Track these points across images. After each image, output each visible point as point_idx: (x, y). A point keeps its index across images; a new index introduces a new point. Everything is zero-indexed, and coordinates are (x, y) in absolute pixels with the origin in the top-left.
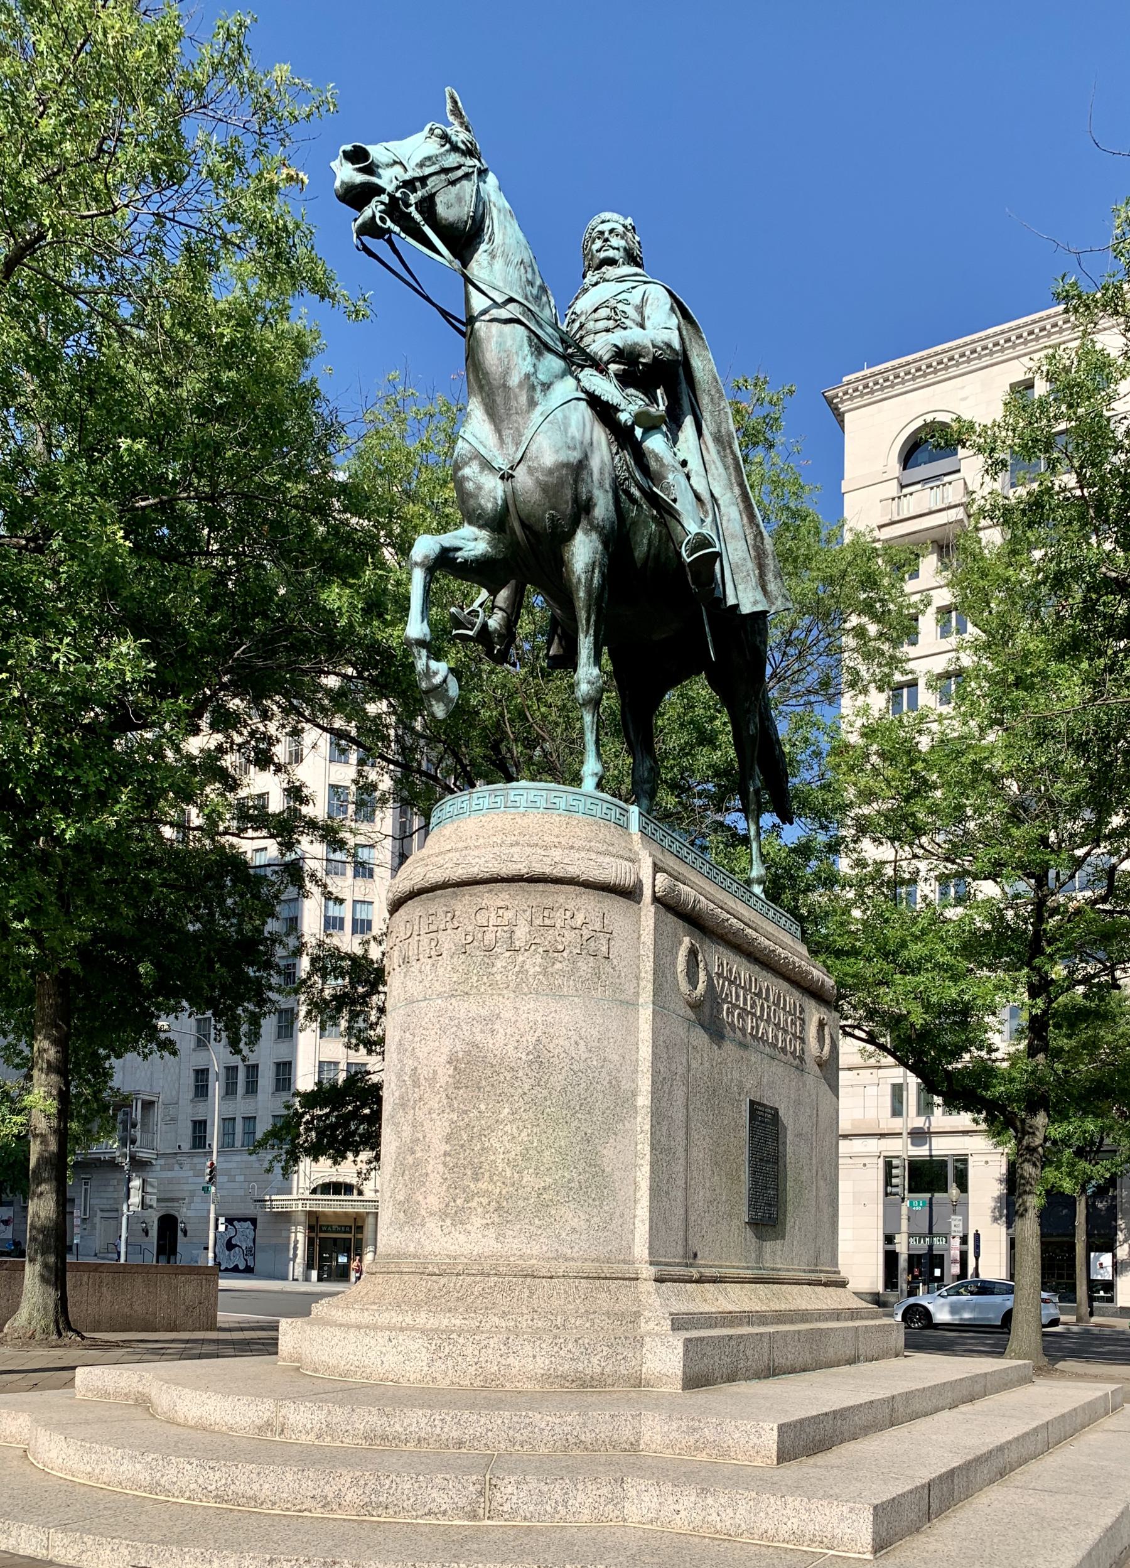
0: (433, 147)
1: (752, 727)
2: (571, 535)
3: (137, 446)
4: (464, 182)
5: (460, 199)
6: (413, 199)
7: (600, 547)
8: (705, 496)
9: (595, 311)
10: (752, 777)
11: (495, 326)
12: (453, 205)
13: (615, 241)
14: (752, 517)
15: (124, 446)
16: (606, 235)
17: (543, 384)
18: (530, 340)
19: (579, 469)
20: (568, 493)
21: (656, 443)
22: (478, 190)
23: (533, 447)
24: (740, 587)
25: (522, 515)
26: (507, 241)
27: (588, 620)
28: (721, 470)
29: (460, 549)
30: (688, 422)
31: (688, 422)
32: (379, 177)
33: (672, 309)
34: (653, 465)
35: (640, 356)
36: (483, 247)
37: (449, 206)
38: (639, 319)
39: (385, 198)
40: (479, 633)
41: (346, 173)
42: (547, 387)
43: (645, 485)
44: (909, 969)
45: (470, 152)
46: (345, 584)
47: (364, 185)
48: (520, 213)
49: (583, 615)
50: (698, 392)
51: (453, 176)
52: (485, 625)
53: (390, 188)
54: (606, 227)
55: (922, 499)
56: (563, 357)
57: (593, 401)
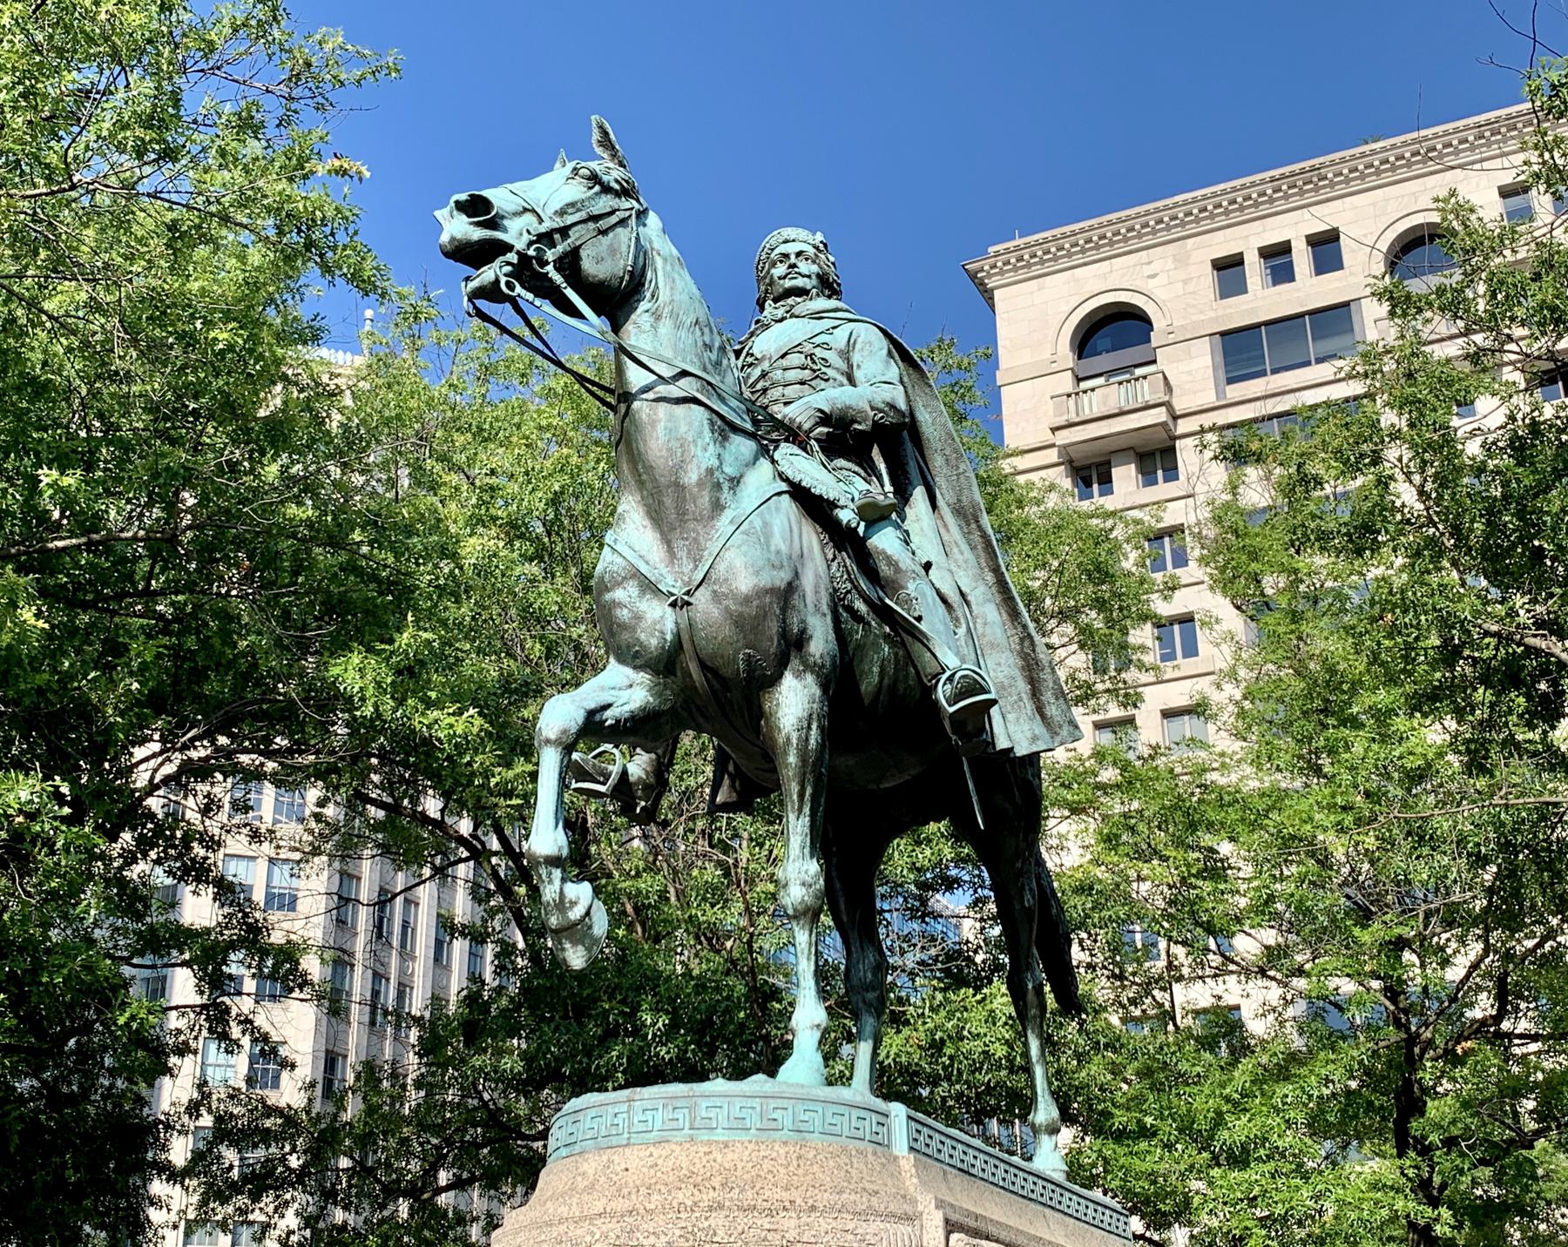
0: (577, 191)
1: (1028, 896)
2: (776, 679)
3: (67, 481)
4: (619, 230)
5: (613, 251)
6: (550, 255)
7: (818, 692)
8: (954, 597)
9: (783, 357)
10: (1029, 967)
11: (663, 406)
12: (604, 260)
13: (804, 267)
14: (1014, 614)
15: (46, 480)
16: (793, 259)
17: (731, 480)
18: (712, 423)
19: (787, 594)
20: (774, 627)
21: (885, 541)
22: (638, 239)
23: (721, 567)
24: (1010, 717)
25: (703, 654)
26: (677, 297)
27: (801, 795)
28: (968, 554)
29: (609, 706)
30: (919, 494)
31: (919, 494)
32: (505, 230)
33: (890, 354)
34: (884, 570)
35: (854, 421)
36: (644, 306)
37: (599, 260)
38: (844, 367)
39: (512, 257)
40: (616, 788)
41: (459, 227)
42: (735, 482)
43: (873, 596)
44: (1239, 1158)
45: (626, 192)
46: (370, 650)
47: (483, 243)
48: (691, 260)
49: (794, 788)
50: (927, 452)
51: (603, 224)
52: (624, 773)
53: (520, 245)
54: (792, 248)
55: (1104, 396)
56: (752, 436)
57: (800, 494)
